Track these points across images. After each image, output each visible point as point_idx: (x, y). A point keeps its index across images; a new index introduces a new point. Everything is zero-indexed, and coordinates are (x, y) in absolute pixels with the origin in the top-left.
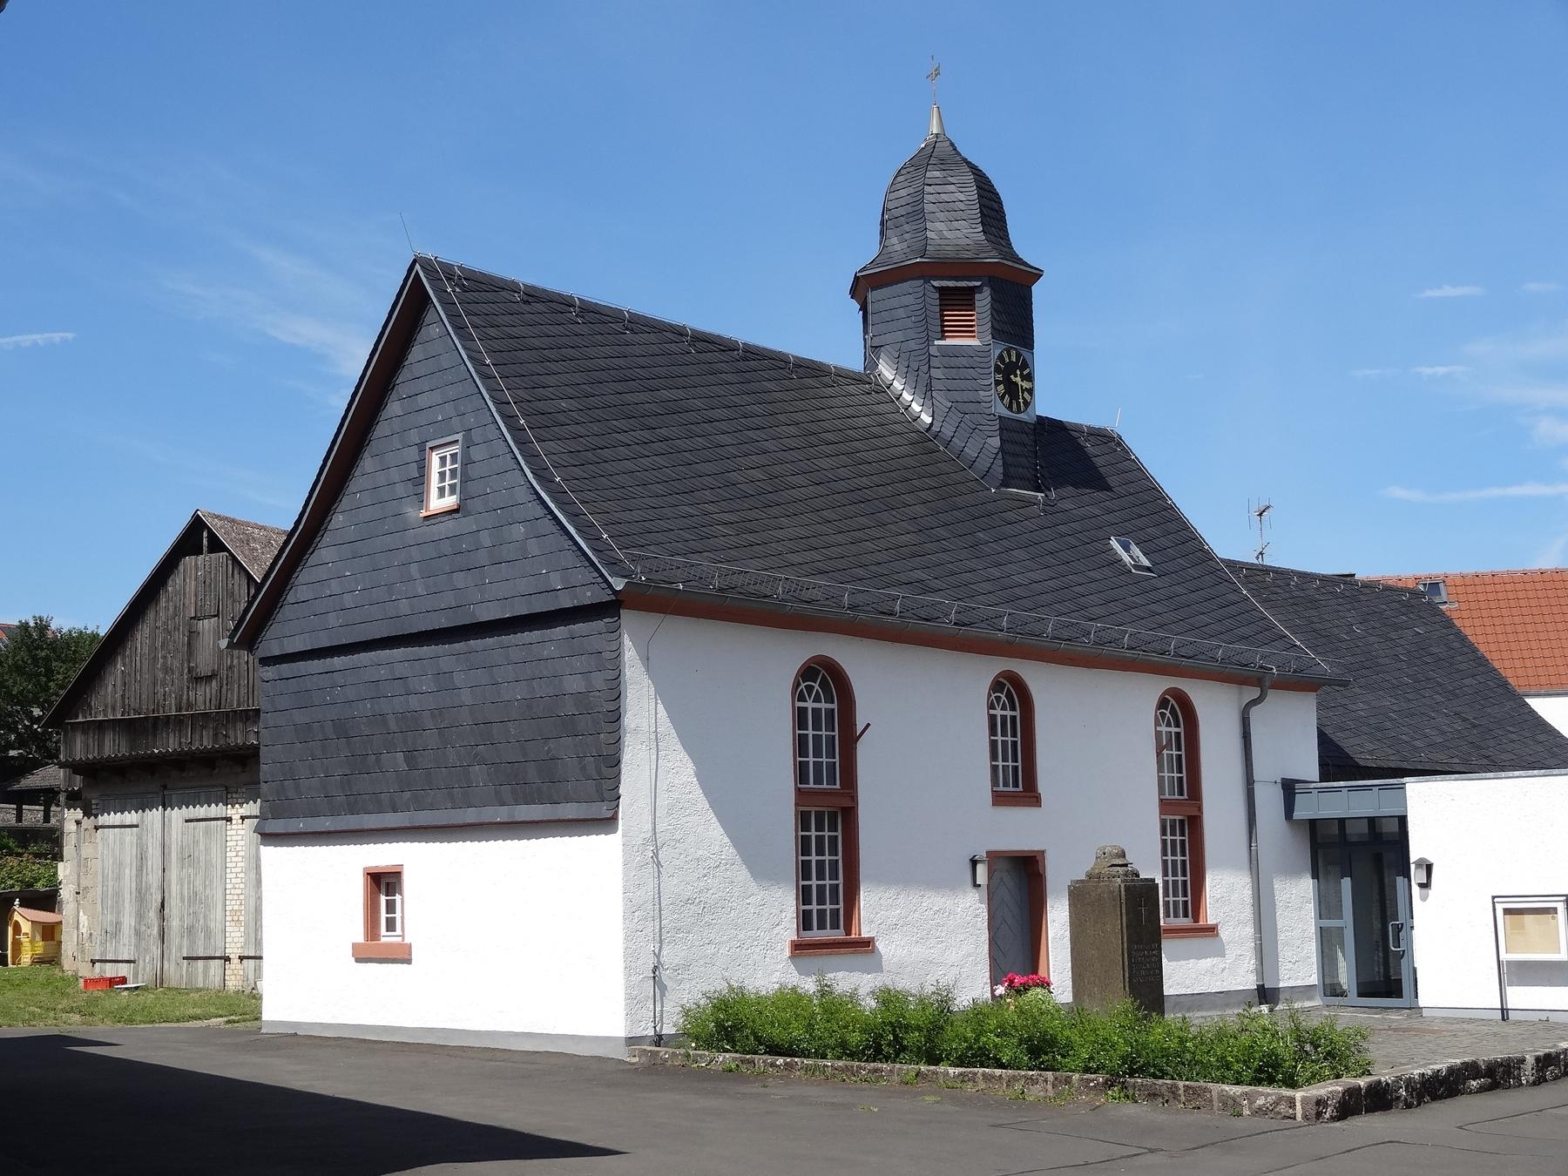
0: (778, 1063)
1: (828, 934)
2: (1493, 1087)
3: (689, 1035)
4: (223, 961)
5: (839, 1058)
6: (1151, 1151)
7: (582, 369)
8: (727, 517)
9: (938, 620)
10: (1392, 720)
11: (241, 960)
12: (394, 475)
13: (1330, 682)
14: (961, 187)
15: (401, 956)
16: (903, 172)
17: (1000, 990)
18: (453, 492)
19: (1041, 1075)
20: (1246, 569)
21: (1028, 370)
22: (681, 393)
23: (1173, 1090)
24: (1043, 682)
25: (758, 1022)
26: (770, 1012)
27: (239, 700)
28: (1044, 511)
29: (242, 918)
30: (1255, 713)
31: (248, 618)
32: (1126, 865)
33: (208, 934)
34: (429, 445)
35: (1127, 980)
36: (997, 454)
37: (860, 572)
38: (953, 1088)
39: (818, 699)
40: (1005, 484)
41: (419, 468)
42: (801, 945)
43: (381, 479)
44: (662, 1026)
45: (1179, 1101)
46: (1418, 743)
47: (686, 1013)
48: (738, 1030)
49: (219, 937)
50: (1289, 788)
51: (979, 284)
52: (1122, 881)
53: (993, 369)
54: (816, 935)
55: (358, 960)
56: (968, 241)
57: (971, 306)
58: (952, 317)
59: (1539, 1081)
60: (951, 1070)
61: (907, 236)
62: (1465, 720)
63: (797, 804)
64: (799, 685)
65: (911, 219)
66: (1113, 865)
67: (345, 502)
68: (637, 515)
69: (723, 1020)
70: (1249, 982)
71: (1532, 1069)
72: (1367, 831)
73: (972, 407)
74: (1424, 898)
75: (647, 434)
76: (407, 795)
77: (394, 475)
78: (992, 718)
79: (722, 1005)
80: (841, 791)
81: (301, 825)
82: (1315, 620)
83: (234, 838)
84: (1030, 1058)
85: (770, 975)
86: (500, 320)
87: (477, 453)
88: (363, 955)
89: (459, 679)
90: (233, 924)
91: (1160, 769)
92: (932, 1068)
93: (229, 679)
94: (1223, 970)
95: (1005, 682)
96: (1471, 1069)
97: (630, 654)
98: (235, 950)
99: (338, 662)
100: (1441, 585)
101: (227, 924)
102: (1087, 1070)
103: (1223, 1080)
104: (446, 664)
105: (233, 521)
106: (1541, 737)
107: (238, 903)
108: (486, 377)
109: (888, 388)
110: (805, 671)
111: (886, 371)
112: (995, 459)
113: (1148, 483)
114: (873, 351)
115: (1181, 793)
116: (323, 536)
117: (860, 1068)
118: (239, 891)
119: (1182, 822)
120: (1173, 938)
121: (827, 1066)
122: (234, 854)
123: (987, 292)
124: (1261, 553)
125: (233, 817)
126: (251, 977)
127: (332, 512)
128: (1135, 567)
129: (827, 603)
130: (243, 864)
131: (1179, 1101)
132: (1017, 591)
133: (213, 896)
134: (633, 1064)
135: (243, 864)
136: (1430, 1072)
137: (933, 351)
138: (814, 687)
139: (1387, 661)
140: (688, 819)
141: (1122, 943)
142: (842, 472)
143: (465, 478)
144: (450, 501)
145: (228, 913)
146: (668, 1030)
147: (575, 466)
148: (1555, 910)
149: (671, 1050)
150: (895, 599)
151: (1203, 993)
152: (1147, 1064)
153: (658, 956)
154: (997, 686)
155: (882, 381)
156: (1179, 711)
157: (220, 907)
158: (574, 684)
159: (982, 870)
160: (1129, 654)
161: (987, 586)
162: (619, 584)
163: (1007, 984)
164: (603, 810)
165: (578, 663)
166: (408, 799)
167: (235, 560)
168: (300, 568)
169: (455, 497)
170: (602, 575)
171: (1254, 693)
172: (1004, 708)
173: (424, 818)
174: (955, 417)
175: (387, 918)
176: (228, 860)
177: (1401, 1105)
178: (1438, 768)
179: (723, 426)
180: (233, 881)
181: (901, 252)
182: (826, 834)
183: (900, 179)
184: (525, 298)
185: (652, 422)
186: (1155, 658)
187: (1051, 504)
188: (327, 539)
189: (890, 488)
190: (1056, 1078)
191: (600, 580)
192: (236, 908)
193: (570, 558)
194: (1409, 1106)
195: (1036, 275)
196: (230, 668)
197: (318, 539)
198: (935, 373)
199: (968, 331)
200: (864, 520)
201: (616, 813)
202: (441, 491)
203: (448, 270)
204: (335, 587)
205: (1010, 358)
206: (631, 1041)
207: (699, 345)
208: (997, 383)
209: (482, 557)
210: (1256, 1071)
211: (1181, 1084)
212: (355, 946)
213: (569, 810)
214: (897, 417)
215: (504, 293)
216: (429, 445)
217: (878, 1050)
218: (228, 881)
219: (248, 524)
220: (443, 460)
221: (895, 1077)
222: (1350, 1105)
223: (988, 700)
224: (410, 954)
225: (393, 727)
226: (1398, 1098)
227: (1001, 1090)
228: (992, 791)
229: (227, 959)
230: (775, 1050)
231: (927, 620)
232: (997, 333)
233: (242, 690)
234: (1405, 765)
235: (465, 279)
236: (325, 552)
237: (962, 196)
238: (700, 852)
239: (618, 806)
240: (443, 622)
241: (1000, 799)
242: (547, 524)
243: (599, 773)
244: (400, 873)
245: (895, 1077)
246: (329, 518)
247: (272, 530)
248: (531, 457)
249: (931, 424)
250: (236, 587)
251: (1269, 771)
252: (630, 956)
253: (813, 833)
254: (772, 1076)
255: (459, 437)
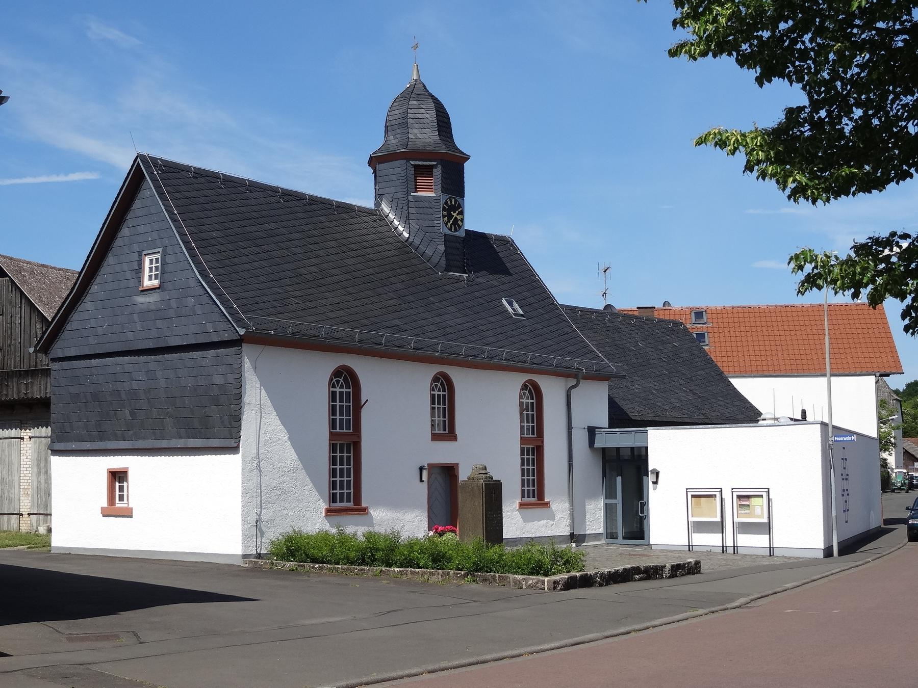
0: (316, 566)
1: (345, 505)
2: (648, 578)
3: (273, 554)
4: (19, 516)
5: (346, 564)
6: (475, 601)
7: (224, 214)
8: (297, 293)
9: (404, 347)
10: (653, 394)
11: (29, 515)
12: (125, 267)
13: (616, 376)
14: (428, 109)
15: (127, 514)
16: (397, 100)
17: (431, 533)
18: (156, 278)
19: (436, 571)
20: (581, 311)
21: (461, 209)
22: (275, 225)
23: (494, 578)
24: (458, 376)
25: (307, 547)
26: (313, 542)
27: (15, 365)
28: (467, 284)
29: (29, 493)
30: (574, 393)
31: (45, 337)
32: (487, 474)
33: (10, 501)
34: (144, 253)
35: (484, 528)
36: (443, 254)
37: (366, 322)
38: (397, 577)
39: (342, 387)
40: (447, 270)
41: (138, 264)
42: (331, 510)
43: (118, 268)
44: (261, 549)
45: (496, 583)
46: (665, 407)
47: (272, 543)
48: (297, 551)
49: (16, 503)
50: (592, 432)
51: (435, 163)
52: (483, 481)
53: (441, 208)
54: (338, 505)
55: (104, 516)
56: (430, 140)
57: (431, 175)
58: (421, 180)
59: (673, 576)
60: (396, 569)
61: (398, 136)
62: (695, 394)
63: (329, 440)
64: (332, 380)
65: (400, 127)
66: (480, 474)
67: (98, 279)
68: (251, 294)
69: (290, 546)
70: (566, 531)
71: (669, 571)
72: (630, 454)
73: (430, 229)
74: (655, 489)
75: (257, 249)
76: (131, 432)
77: (125, 267)
78: (433, 397)
79: (289, 539)
80: (353, 433)
81: (74, 446)
82: (617, 339)
83: (25, 449)
84: (433, 564)
85: (315, 525)
86: (181, 188)
87: (169, 259)
88: (106, 513)
89: (159, 374)
90: (24, 496)
91: (522, 421)
92: (388, 568)
93: (9, 353)
94: (552, 525)
95: (529, 385)
96: (636, 570)
97: (247, 364)
98: (26, 510)
99: (94, 362)
100: (704, 313)
101: (21, 495)
102: (458, 569)
103: (516, 573)
104: (152, 366)
105: (11, 259)
106: (737, 403)
107: (27, 484)
108: (175, 221)
109: (386, 217)
110: (336, 372)
111: (385, 208)
112: (441, 257)
113: (526, 267)
114: (379, 196)
115: (533, 434)
116: (86, 296)
117: (354, 568)
118: (28, 478)
119: (533, 449)
120: (544, 507)
121: (339, 568)
122: (25, 457)
123: (440, 167)
124: (605, 293)
125: (25, 437)
126: (35, 525)
127: (91, 284)
128: (514, 314)
129: (346, 339)
130: (30, 463)
131: (496, 583)
132: (448, 330)
133: (13, 480)
134: (246, 567)
135: (30, 463)
136: (613, 571)
137: (410, 198)
138: (340, 381)
139: (655, 361)
140: (275, 447)
141: (483, 511)
142: (359, 266)
143: (163, 271)
144: (155, 283)
145: (21, 490)
146: (264, 551)
147: (220, 268)
148: (715, 496)
149: (264, 561)
150: (382, 336)
151: (541, 537)
152: (484, 566)
153: (260, 516)
154: (436, 379)
155: (383, 213)
156: (534, 392)
157: (17, 486)
158: (218, 380)
159: (425, 473)
160: (505, 363)
161: (433, 327)
162: (242, 332)
163: (434, 531)
164: (232, 443)
165: (221, 369)
166: (132, 434)
167: (13, 282)
168: (73, 312)
169: (158, 280)
170: (233, 326)
171: (573, 382)
172: (439, 391)
173: (140, 444)
174: (421, 234)
175: (119, 495)
176: (22, 461)
177: (597, 585)
178: (675, 421)
179: (296, 243)
180: (25, 472)
181: (395, 145)
182: (345, 455)
183: (396, 104)
184: (195, 175)
185: (258, 241)
186: (519, 365)
187: (471, 280)
188: (88, 298)
189: (384, 274)
190: (443, 573)
191: (232, 328)
192: (26, 487)
193: (216, 317)
194: (601, 585)
195: (467, 158)
196: (10, 345)
197: (83, 298)
198: (411, 210)
199: (429, 188)
200: (370, 293)
201: (239, 445)
202: (150, 278)
203: (154, 160)
204: (93, 323)
205: (451, 202)
206: (245, 556)
207: (285, 197)
208: (444, 216)
209: (172, 313)
210: (531, 569)
211: (497, 575)
212: (102, 509)
213: (215, 443)
214: (390, 234)
215: (183, 173)
216: (144, 253)
217: (364, 560)
218: (22, 472)
219: (20, 261)
220: (151, 261)
221: (371, 573)
222: (571, 584)
223: (430, 387)
224: (132, 513)
225: (124, 396)
226: (596, 582)
227: (418, 578)
228: (432, 433)
229: (21, 515)
230: (314, 560)
231: (399, 347)
232: (445, 190)
233: (17, 358)
234: (657, 419)
235: (163, 166)
236: (87, 305)
237: (428, 116)
238: (280, 464)
239: (239, 441)
240: (151, 345)
241: (435, 437)
242: (205, 299)
243: (230, 424)
244: (127, 472)
245: (371, 573)
246: (90, 287)
247: (34, 264)
248: (198, 264)
249: (409, 238)
250: (14, 299)
251: (580, 421)
252: (245, 515)
253: (338, 454)
254: (313, 573)
255: (160, 250)
